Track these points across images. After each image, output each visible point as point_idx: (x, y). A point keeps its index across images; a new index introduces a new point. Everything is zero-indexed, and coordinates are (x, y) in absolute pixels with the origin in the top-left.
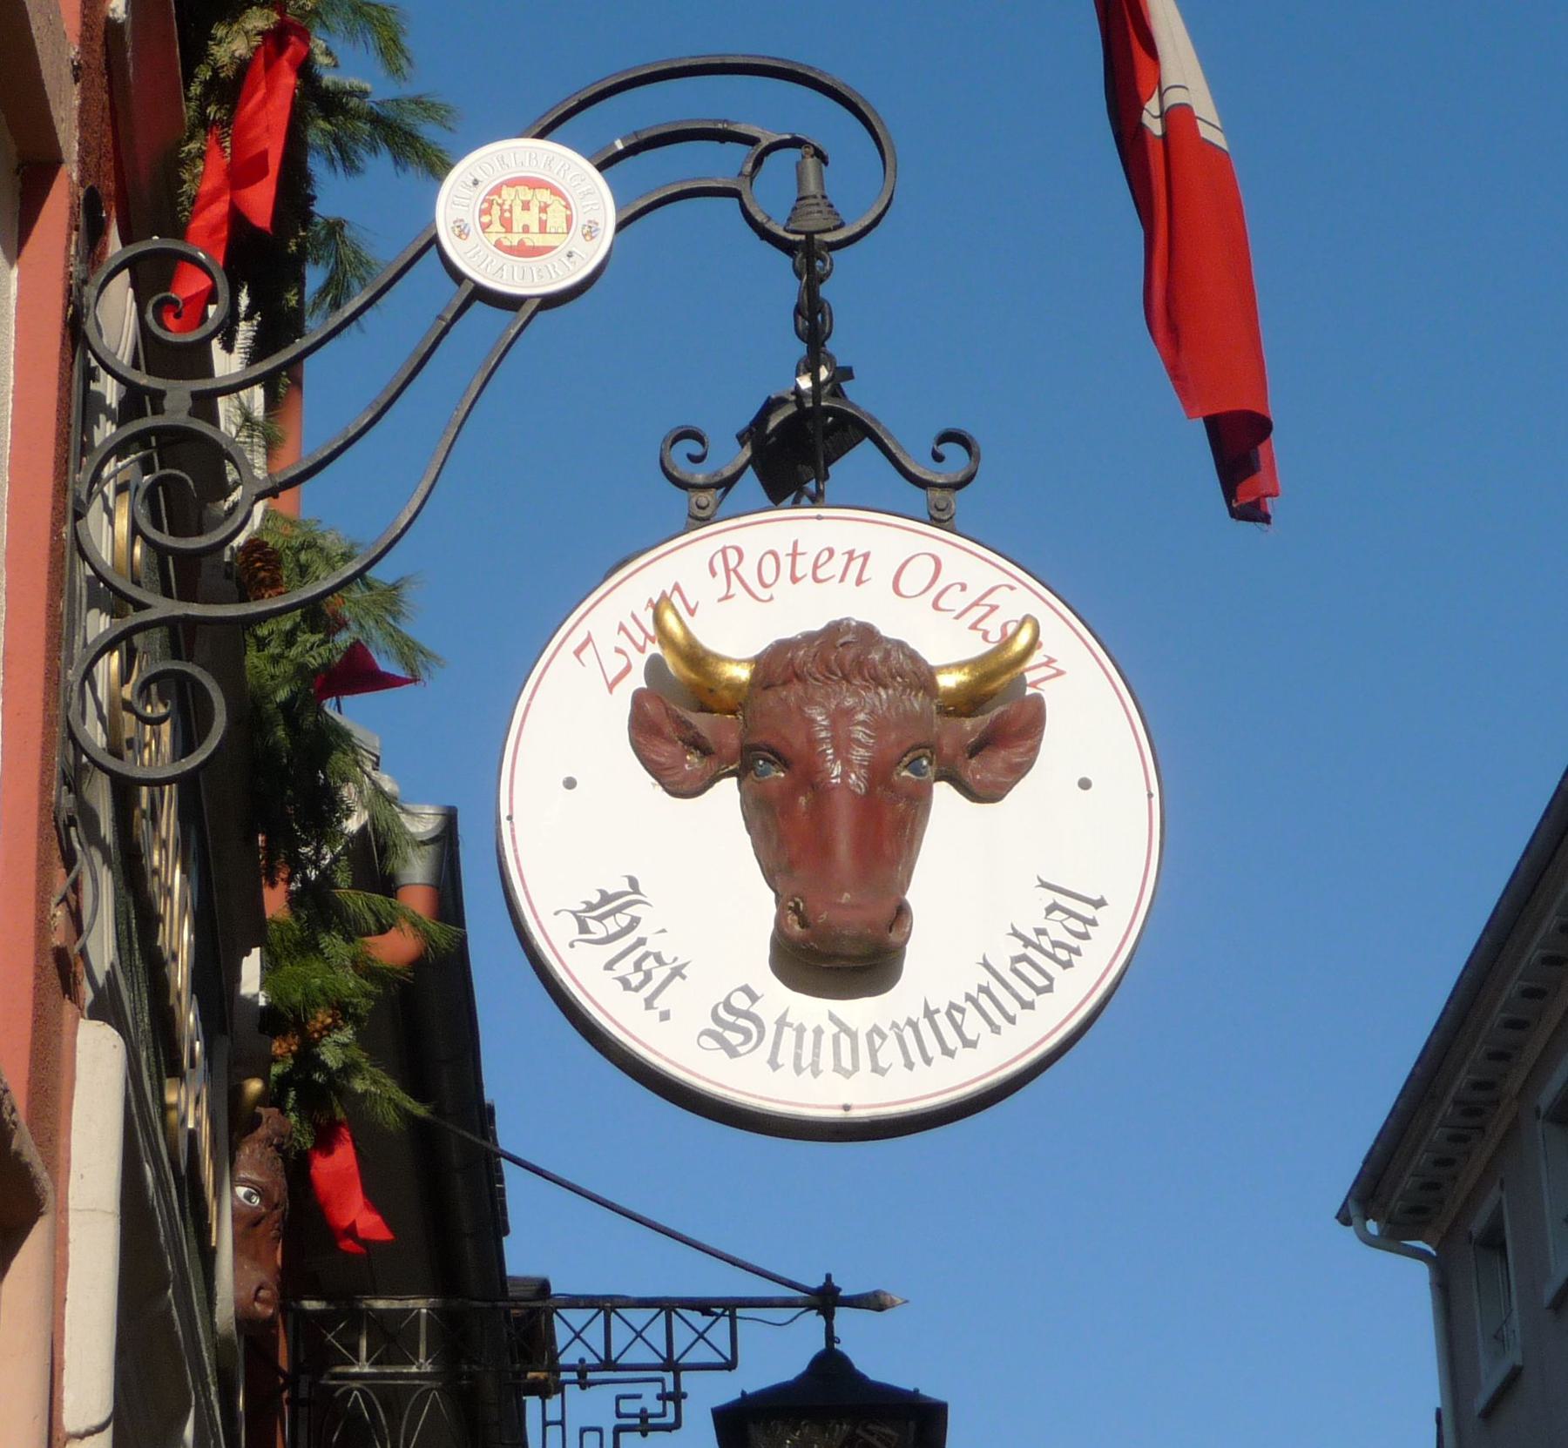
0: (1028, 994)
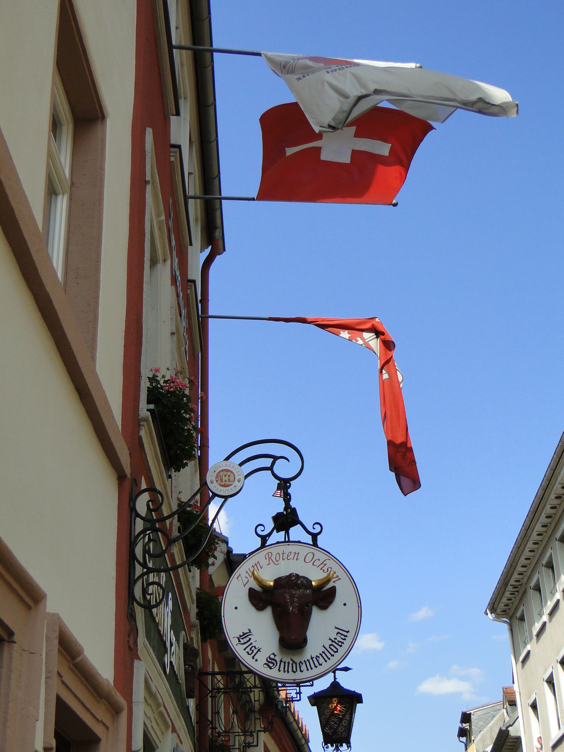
0: (332, 653)
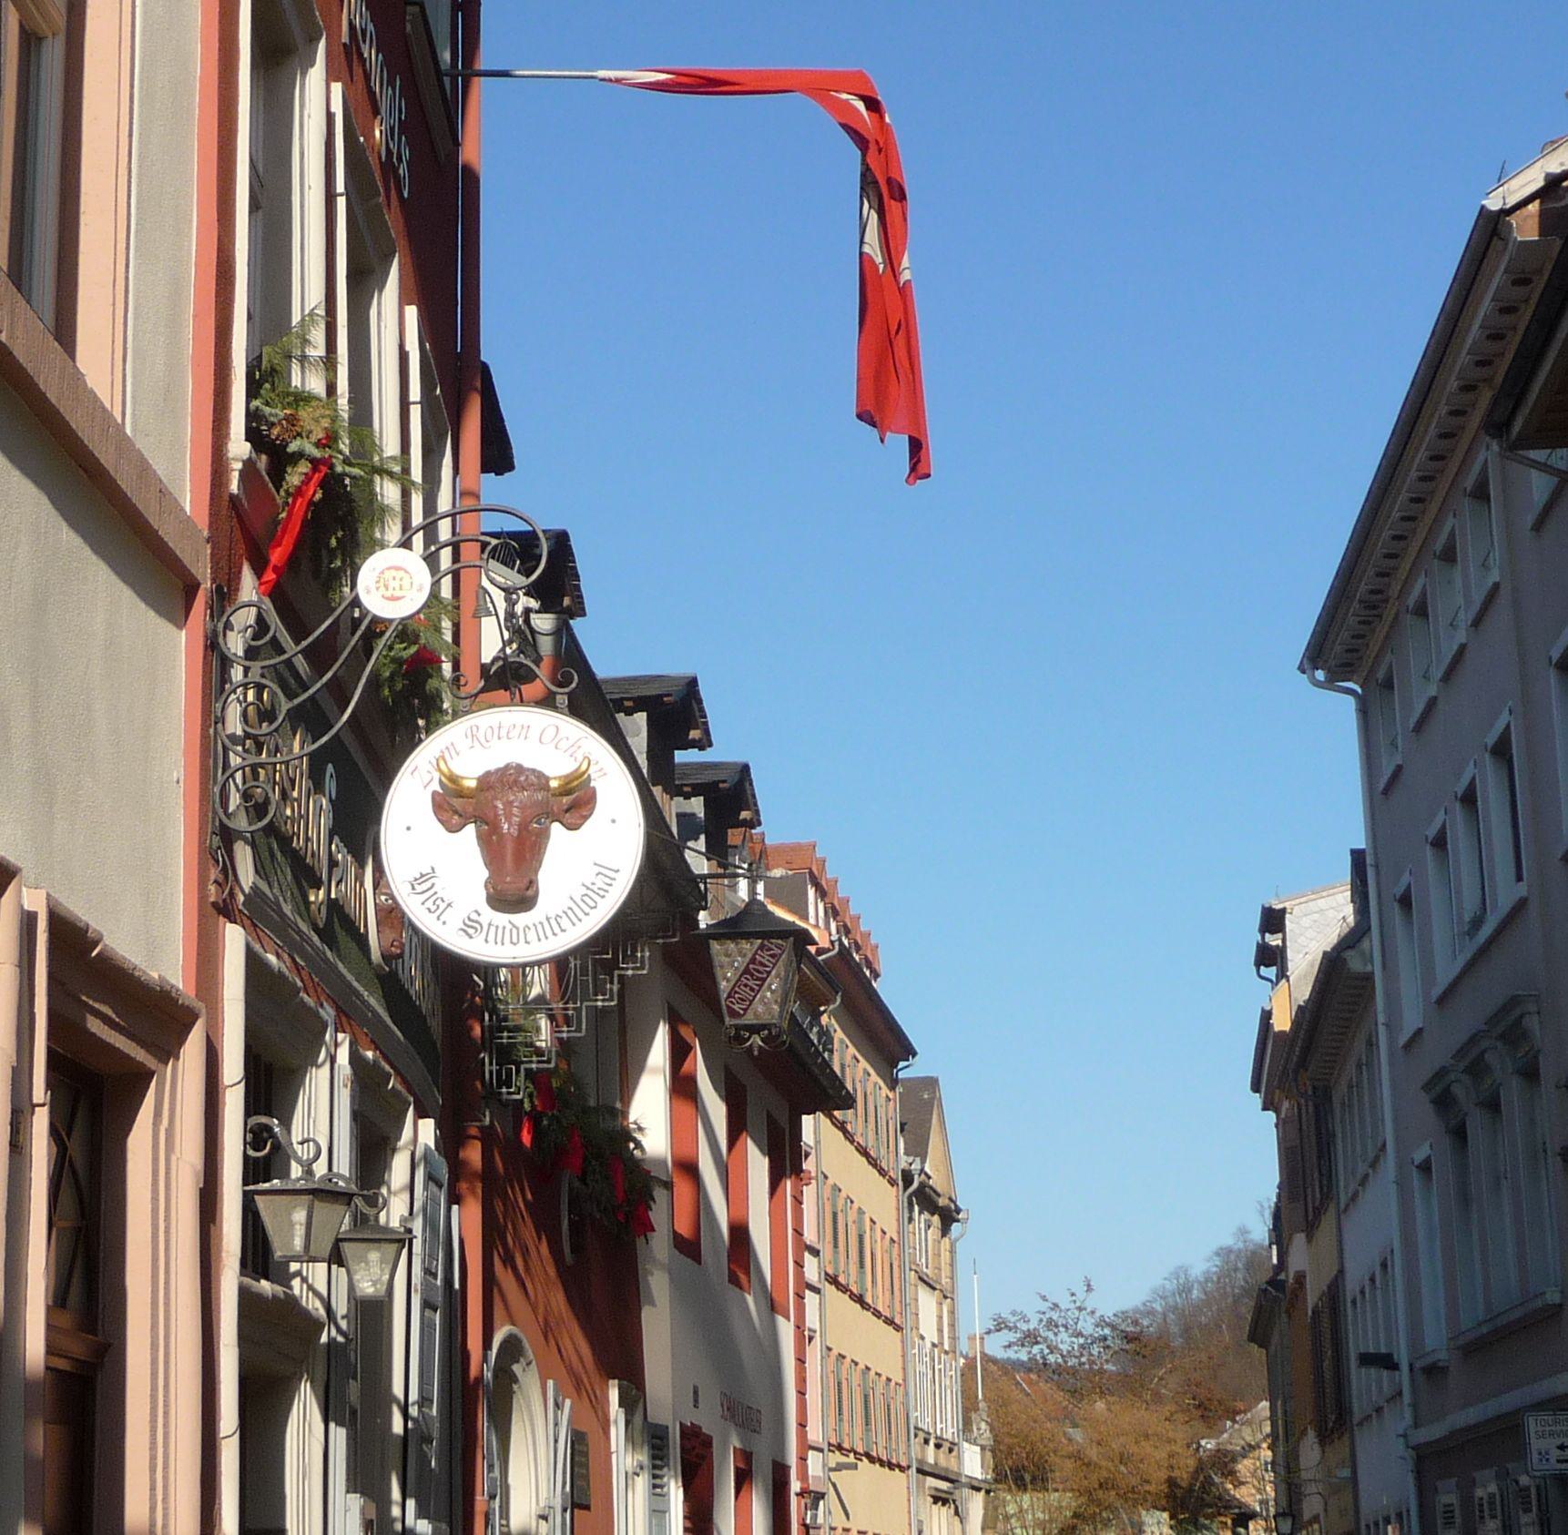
0: (587, 910)
